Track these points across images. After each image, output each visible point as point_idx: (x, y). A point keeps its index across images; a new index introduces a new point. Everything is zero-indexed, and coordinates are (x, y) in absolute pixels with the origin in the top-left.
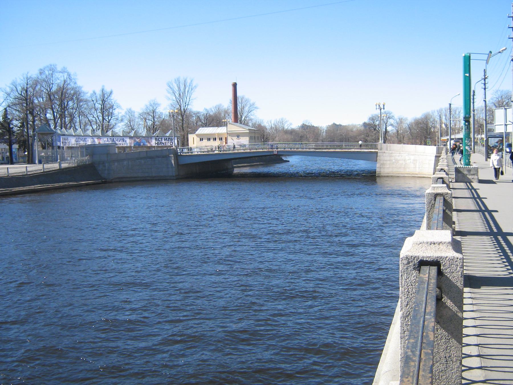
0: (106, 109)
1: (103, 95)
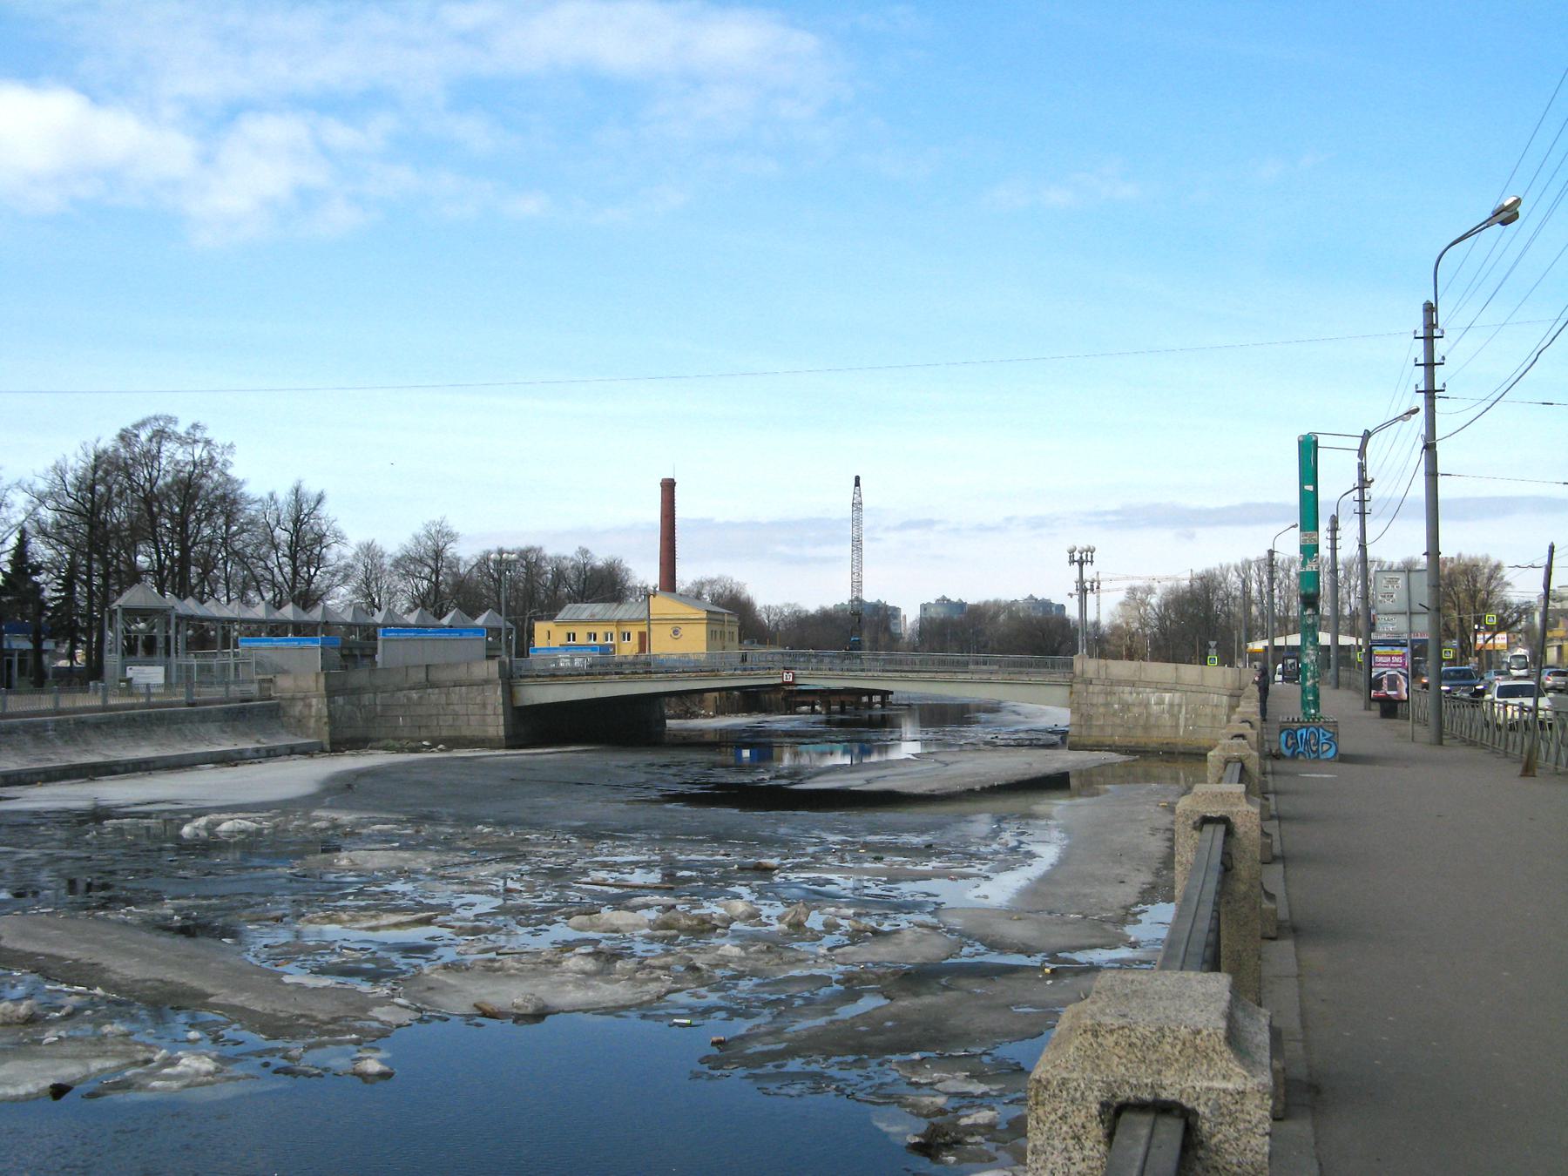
0: (306, 542)
1: (299, 510)
